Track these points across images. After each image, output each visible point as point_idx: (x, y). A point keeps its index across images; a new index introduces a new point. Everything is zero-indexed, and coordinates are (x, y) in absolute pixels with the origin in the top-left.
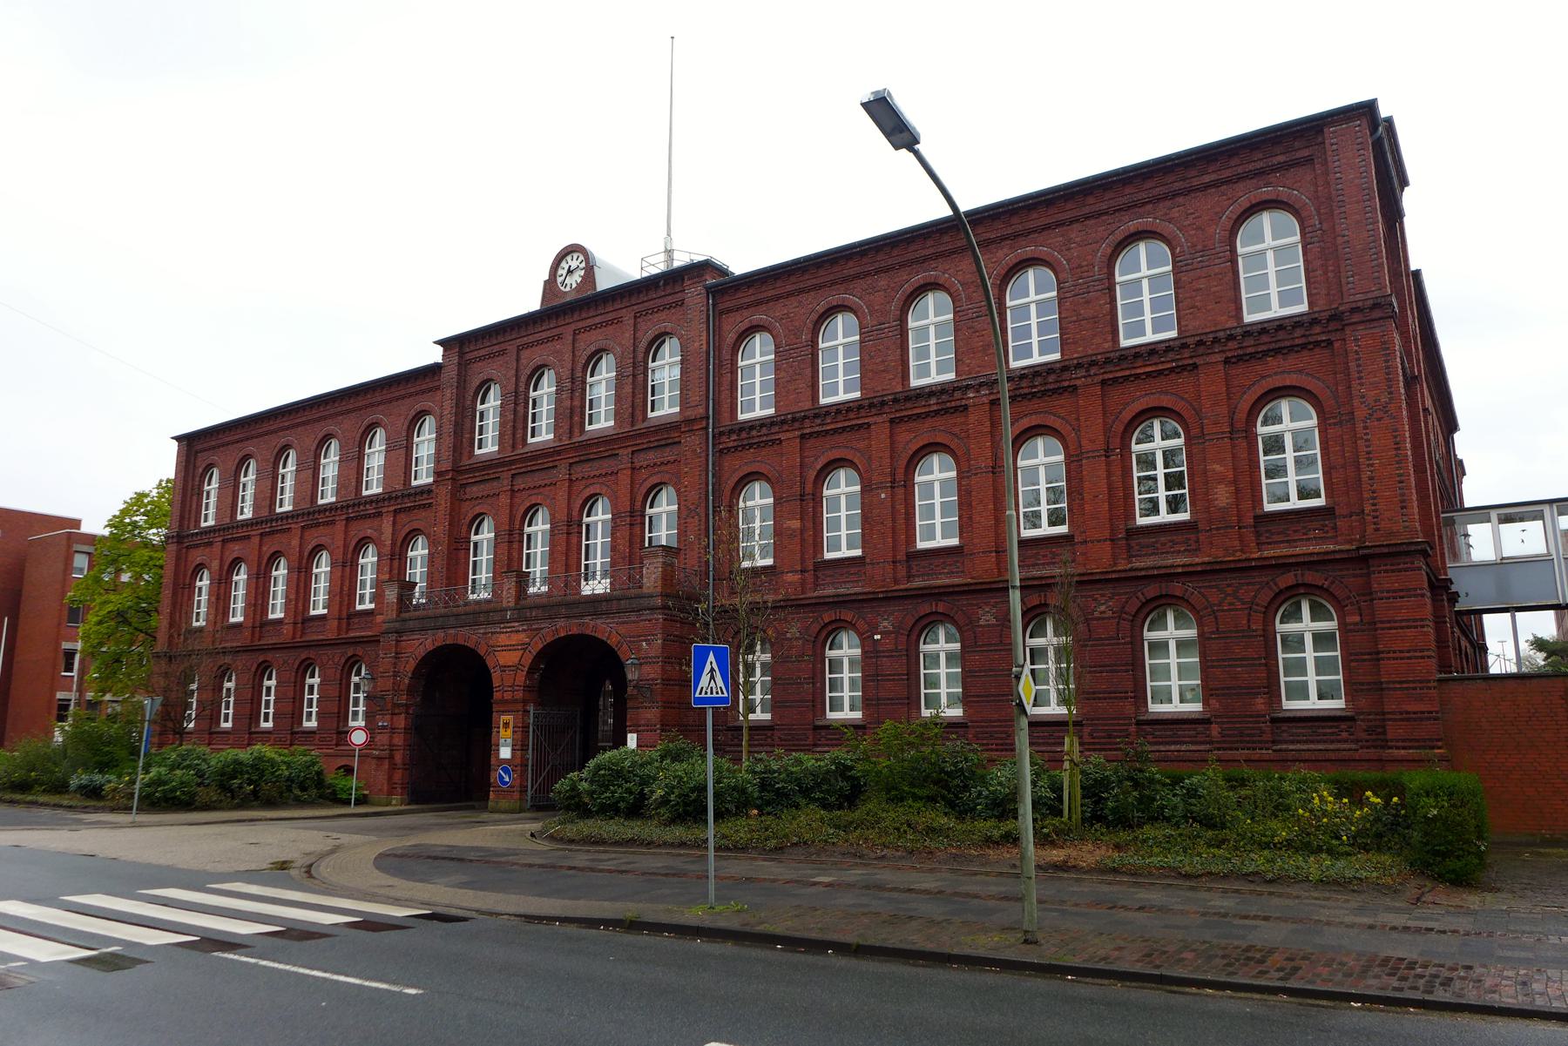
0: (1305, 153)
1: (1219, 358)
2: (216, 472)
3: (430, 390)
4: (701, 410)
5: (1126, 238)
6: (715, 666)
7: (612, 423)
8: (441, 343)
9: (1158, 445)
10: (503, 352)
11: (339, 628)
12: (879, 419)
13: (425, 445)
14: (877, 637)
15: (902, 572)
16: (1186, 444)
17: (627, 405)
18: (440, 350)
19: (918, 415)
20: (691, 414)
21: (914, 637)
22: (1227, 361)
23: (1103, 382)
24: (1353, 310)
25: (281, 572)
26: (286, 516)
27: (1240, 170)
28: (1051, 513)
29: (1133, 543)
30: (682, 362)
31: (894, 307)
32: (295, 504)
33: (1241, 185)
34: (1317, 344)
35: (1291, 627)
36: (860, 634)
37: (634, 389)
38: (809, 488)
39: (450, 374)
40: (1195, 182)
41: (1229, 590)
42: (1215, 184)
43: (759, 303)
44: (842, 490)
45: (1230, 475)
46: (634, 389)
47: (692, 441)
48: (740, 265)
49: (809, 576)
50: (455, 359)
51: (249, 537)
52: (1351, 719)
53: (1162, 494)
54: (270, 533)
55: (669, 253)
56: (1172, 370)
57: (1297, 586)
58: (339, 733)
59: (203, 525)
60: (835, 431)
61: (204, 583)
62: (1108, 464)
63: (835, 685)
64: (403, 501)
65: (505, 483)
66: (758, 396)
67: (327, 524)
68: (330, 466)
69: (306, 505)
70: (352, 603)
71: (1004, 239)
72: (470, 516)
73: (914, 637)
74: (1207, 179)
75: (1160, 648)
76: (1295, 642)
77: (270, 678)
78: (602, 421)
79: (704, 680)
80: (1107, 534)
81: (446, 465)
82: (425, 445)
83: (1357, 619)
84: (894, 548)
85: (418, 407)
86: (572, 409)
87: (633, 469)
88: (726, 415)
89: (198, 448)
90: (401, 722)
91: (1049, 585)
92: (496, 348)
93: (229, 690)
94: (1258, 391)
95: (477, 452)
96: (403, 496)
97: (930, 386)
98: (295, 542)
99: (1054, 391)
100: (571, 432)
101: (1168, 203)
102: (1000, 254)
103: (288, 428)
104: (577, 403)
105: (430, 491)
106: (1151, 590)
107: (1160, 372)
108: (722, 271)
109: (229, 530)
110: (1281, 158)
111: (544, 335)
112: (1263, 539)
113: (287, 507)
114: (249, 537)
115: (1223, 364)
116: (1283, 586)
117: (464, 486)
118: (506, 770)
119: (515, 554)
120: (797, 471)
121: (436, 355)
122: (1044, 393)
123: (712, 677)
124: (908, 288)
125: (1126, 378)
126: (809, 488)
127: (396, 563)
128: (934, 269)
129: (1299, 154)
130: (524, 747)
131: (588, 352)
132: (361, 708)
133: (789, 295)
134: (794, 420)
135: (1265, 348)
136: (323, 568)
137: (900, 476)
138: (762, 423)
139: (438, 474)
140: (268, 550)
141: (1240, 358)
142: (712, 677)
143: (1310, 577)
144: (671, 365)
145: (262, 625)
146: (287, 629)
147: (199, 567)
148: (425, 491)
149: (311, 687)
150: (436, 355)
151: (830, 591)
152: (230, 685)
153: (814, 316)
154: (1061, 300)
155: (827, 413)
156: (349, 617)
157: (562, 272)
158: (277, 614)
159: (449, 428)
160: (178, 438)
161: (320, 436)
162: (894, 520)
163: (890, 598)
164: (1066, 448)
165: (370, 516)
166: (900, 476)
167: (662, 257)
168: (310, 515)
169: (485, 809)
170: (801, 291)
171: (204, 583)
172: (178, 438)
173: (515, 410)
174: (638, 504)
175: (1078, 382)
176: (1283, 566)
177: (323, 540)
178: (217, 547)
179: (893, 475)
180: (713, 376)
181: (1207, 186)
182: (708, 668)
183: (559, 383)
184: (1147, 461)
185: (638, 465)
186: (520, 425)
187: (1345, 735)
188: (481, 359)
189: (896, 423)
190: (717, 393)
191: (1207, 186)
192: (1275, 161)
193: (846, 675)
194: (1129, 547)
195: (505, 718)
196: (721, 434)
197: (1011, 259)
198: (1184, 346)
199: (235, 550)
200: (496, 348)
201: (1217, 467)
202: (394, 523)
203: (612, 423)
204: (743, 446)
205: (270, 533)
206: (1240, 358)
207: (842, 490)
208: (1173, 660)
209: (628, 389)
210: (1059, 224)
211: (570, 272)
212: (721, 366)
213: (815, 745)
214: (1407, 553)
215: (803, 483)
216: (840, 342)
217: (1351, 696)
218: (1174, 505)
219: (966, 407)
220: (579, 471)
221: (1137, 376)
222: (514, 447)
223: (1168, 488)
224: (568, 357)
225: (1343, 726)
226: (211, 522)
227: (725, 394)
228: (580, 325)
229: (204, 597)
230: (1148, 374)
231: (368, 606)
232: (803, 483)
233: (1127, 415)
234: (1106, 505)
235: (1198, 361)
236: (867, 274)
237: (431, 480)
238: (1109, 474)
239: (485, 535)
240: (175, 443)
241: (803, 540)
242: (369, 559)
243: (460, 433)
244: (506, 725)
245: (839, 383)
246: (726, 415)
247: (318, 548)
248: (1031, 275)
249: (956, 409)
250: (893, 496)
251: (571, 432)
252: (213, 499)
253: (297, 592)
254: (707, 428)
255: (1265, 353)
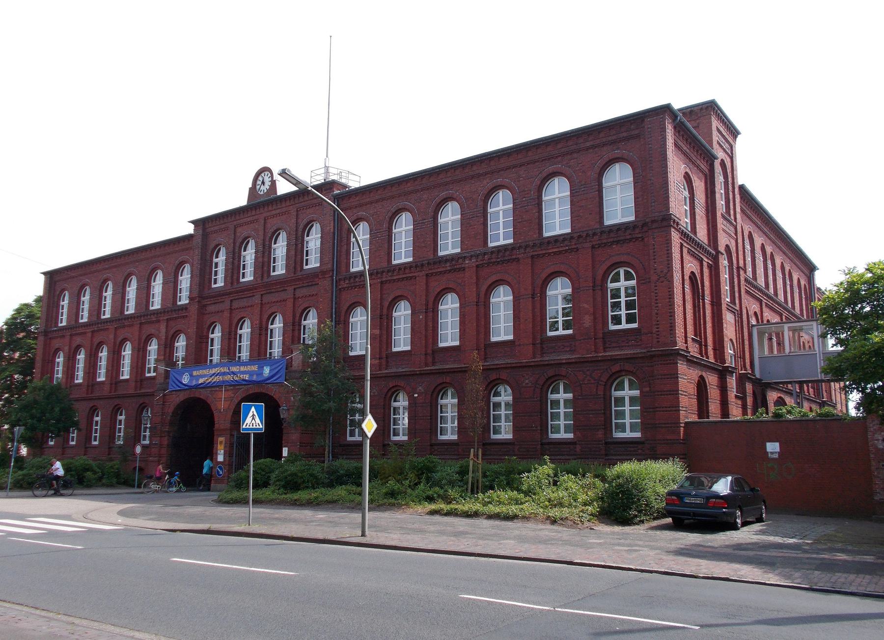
0: (637, 132)
1: (589, 245)
2: (67, 293)
3: (187, 249)
4: (330, 266)
5: (548, 176)
6: (255, 413)
7: (318, 265)
8: (192, 222)
9: (623, 284)
10: (227, 229)
11: (136, 388)
12: (421, 274)
13: (185, 280)
14: (416, 395)
15: (430, 359)
16: (637, 283)
17: (292, 262)
18: (192, 226)
19: (441, 272)
20: (325, 268)
21: (435, 396)
22: (593, 247)
23: (532, 257)
24: (653, 222)
25: (81, 357)
26: (107, 321)
27: (604, 140)
28: (565, 322)
29: (544, 346)
30: (322, 237)
31: (431, 210)
32: (112, 314)
33: (605, 148)
34: (637, 239)
35: (619, 394)
36: (408, 394)
37: (297, 252)
38: (385, 311)
39: (198, 241)
40: (582, 146)
41: (588, 373)
42: (593, 147)
43: (361, 205)
44: (450, 306)
45: (592, 310)
46: (297, 252)
47: (325, 283)
48: (354, 183)
49: (384, 362)
50: (201, 232)
51: (85, 333)
52: (643, 443)
53: (623, 312)
54: (98, 331)
55: (327, 172)
56: (566, 251)
57: (620, 371)
58: (384, 445)
59: (60, 325)
60: (399, 280)
61: (60, 360)
62: (533, 302)
63: (497, 418)
64: (172, 312)
65: (227, 304)
66: (501, 231)
67: (129, 326)
68: (157, 287)
69: (117, 315)
70: (143, 372)
71: (486, 173)
72: (209, 323)
73: (435, 396)
74: (588, 144)
75: (620, 401)
76: (555, 403)
77: (121, 415)
78: (280, 269)
79: (249, 420)
80: (531, 341)
81: (195, 294)
82: (185, 280)
83: (648, 389)
84: (426, 347)
85: (180, 259)
86: (263, 263)
87: (295, 298)
88: (344, 269)
89: (56, 280)
90: (165, 441)
91: (465, 371)
92: (223, 226)
93: (97, 422)
94: (608, 263)
95: (214, 286)
96: (172, 311)
97: (447, 255)
98: (112, 336)
99: (508, 261)
100: (262, 276)
101: (569, 157)
102: (485, 182)
103: (107, 269)
104: (266, 260)
105: (186, 309)
106: (551, 372)
107: (560, 252)
108: (345, 186)
109: (74, 327)
110: (625, 134)
111: (249, 219)
112: (607, 345)
113: (85, 320)
114: (222, 311)
115: (594, 246)
116: (614, 371)
117: (205, 306)
118: (220, 468)
119: (232, 346)
120: (379, 302)
121: (190, 229)
122: (503, 262)
123: (253, 419)
124: (438, 200)
125: (544, 255)
126: (385, 311)
127: (168, 350)
128: (452, 189)
129: (633, 133)
130: (231, 455)
131: (272, 230)
132: (148, 434)
133: (377, 201)
134: (377, 273)
135: (612, 240)
136: (127, 352)
137: (431, 305)
138: (505, 248)
139: (191, 298)
140: (96, 341)
141: (600, 246)
142: (253, 419)
143: (627, 366)
144: (316, 239)
145: (141, 381)
146: (107, 388)
147: (57, 350)
148: (184, 308)
149: (120, 421)
150: (190, 229)
151: (394, 370)
152: (98, 419)
153: (390, 214)
154: (514, 209)
155: (549, 243)
156: (434, 352)
157: (259, 182)
158: (102, 378)
159: (197, 272)
160: (44, 273)
161: (126, 273)
162: (426, 330)
163: (422, 374)
164: (513, 293)
165: (153, 322)
166: (431, 305)
167: (323, 171)
168: (120, 319)
169: (209, 490)
170: (383, 199)
171: (60, 360)
172: (44, 273)
173: (233, 263)
174: (264, 323)
175: (520, 256)
176: (614, 360)
177: (153, 331)
178: (67, 339)
179: (427, 305)
180: (338, 244)
181: (588, 149)
182: (251, 414)
183: (288, 239)
184: (616, 294)
185: (297, 296)
186: (236, 272)
187: (640, 451)
188: (215, 232)
189: (429, 276)
190: (339, 257)
191: (588, 149)
192: (621, 135)
193: (562, 410)
194: (542, 348)
195: (221, 439)
196: (340, 280)
197: (490, 185)
198: (572, 238)
199: (78, 340)
200: (223, 226)
201: (586, 306)
202: (167, 326)
203: (284, 272)
204: (352, 287)
205: (98, 331)
206: (600, 246)
207: (450, 306)
208: (627, 408)
209: (293, 253)
210: (515, 167)
211: (263, 183)
212: (341, 241)
213: (606, 455)
214: (671, 354)
215: (382, 309)
216: (501, 209)
217: (643, 431)
218: (630, 319)
219: (464, 269)
220: (267, 298)
221: (549, 254)
222: (232, 283)
223: (627, 309)
224: (261, 233)
225: (640, 446)
226: (64, 324)
227: (344, 256)
228: (268, 214)
229: (61, 368)
230: (555, 253)
231: (153, 374)
232: (382, 309)
233: (544, 276)
234: (531, 326)
235: (579, 246)
236: (417, 191)
237: (187, 302)
238: (534, 308)
239: (217, 335)
240: (43, 276)
241: (381, 341)
242: (153, 347)
243: (203, 275)
244: (221, 442)
245: (501, 232)
246: (344, 269)
247: (124, 340)
248: (556, 180)
249: (459, 269)
250: (426, 317)
251: (262, 276)
252: (65, 310)
253: (113, 366)
254: (332, 276)
255: (612, 243)
